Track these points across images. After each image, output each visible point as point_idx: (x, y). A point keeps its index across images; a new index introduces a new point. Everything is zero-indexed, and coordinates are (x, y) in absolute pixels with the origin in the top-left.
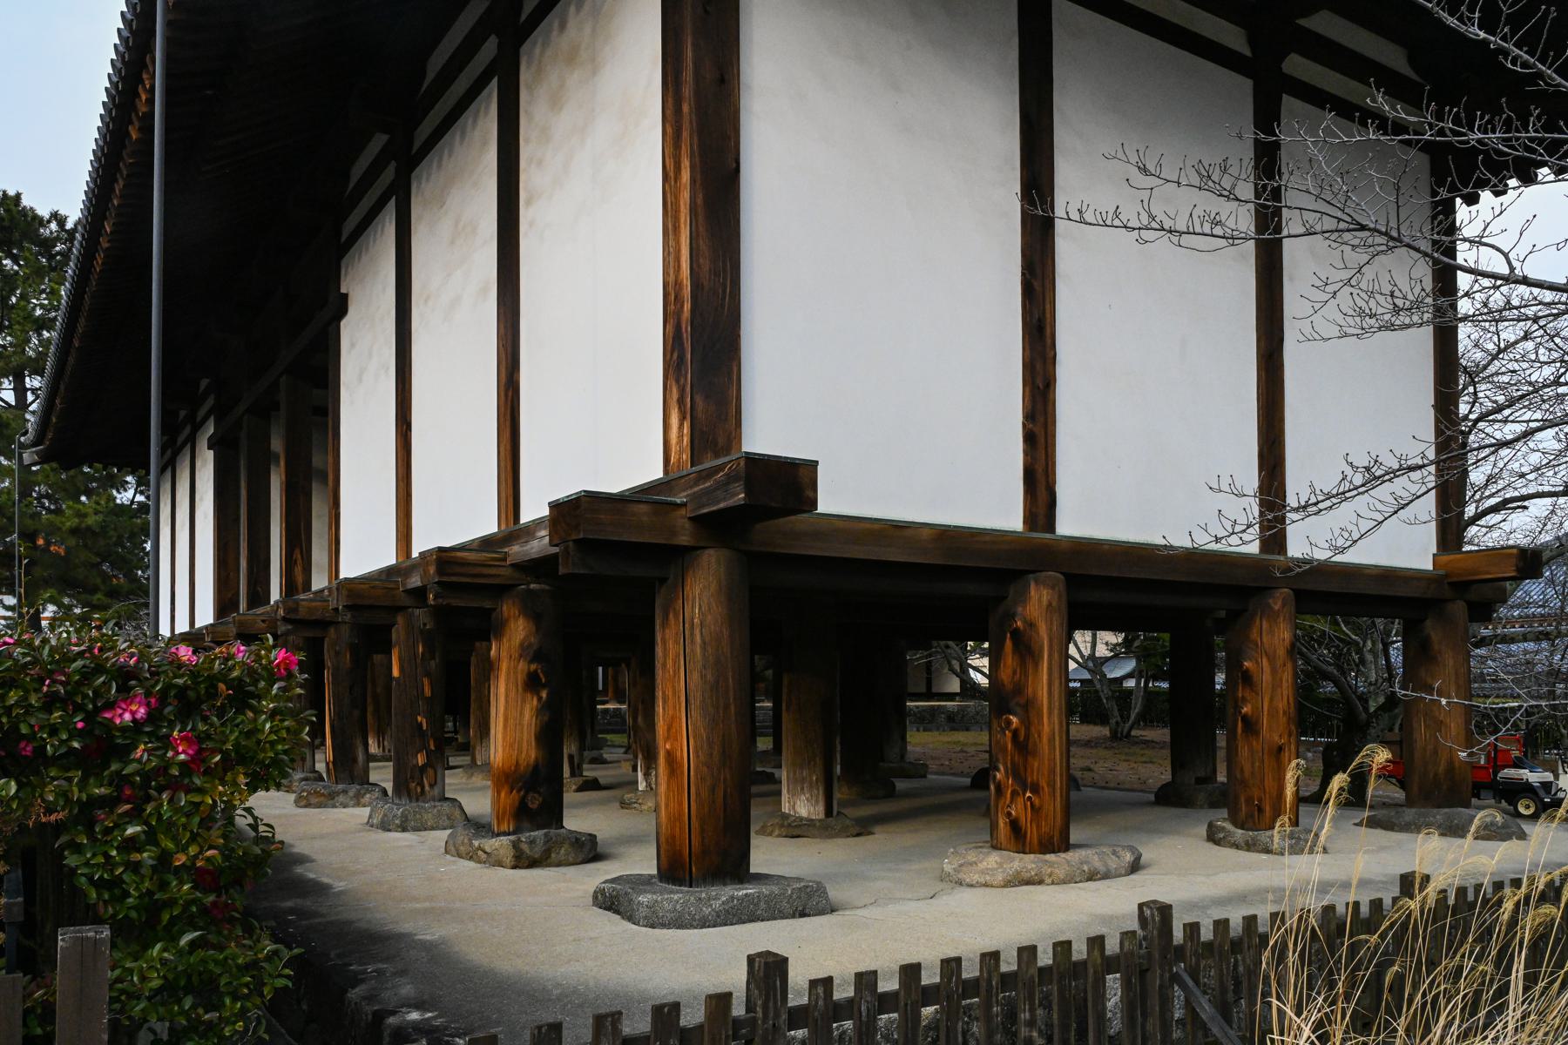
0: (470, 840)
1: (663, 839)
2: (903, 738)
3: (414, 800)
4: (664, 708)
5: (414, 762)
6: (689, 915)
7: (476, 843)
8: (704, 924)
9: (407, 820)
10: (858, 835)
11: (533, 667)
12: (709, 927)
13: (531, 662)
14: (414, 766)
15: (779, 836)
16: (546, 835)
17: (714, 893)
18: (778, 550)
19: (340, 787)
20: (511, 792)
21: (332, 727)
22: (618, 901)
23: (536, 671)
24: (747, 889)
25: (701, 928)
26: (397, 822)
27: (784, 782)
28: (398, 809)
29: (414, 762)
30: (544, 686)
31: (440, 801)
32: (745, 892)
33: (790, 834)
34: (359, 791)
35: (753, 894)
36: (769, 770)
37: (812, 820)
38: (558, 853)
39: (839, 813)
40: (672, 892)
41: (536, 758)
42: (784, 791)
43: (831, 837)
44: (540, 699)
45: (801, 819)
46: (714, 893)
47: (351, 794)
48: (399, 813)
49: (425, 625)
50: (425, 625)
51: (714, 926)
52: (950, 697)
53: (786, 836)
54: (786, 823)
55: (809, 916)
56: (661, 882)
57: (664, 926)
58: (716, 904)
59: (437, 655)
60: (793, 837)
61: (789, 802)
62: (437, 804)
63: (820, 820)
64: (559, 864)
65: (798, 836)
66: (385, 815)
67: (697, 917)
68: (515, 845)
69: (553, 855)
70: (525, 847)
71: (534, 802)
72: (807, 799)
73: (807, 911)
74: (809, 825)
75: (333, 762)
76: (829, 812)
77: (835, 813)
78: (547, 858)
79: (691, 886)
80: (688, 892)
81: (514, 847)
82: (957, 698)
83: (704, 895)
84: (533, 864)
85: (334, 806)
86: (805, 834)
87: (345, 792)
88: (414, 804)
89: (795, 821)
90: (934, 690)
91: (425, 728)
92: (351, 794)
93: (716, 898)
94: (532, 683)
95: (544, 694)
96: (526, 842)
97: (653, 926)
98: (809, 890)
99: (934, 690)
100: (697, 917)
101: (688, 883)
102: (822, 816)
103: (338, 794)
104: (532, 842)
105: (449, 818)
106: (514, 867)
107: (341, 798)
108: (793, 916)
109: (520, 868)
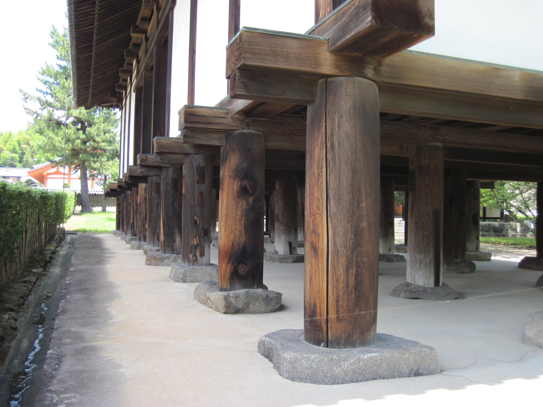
0: (205, 292)
1: (307, 305)
2: (478, 238)
3: (191, 264)
4: (310, 203)
6: (323, 372)
8: (335, 381)
9: (186, 276)
10: (456, 299)
11: (244, 183)
12: (338, 384)
13: (242, 180)
14: (192, 245)
16: (246, 293)
17: (344, 356)
19: (166, 255)
20: (229, 263)
21: (164, 223)
24: (372, 352)
25: (332, 384)
26: (181, 276)
28: (182, 269)
29: (192, 242)
30: (251, 195)
33: (410, 297)
34: (175, 258)
36: (401, 254)
38: (254, 305)
39: (443, 284)
40: (310, 352)
41: (245, 242)
43: (437, 299)
45: (419, 287)
46: (344, 356)
47: (171, 259)
49: (200, 164)
51: (343, 383)
52: (495, 219)
53: (408, 298)
55: (422, 375)
56: (305, 341)
58: (345, 365)
59: (206, 181)
60: (413, 298)
61: (411, 275)
62: (204, 267)
63: (431, 288)
64: (255, 312)
65: (416, 298)
67: (328, 375)
68: (226, 298)
69: (251, 306)
70: (232, 300)
71: (242, 269)
72: (423, 274)
73: (421, 371)
74: (424, 291)
75: (164, 242)
77: (441, 284)
78: (246, 308)
80: (323, 352)
81: (225, 299)
82: (498, 220)
84: (237, 311)
85: (163, 265)
86: (419, 297)
87: (168, 258)
88: (191, 267)
89: (414, 288)
90: (487, 216)
91: (198, 223)
92: (171, 259)
93: (346, 360)
94: (243, 192)
95: (251, 200)
96: (233, 297)
97: (293, 379)
98: (423, 354)
99: (487, 216)
100: (328, 375)
103: (165, 258)
104: (237, 297)
105: (210, 276)
106: (226, 313)
107: (166, 261)
108: (409, 376)
109: (229, 313)
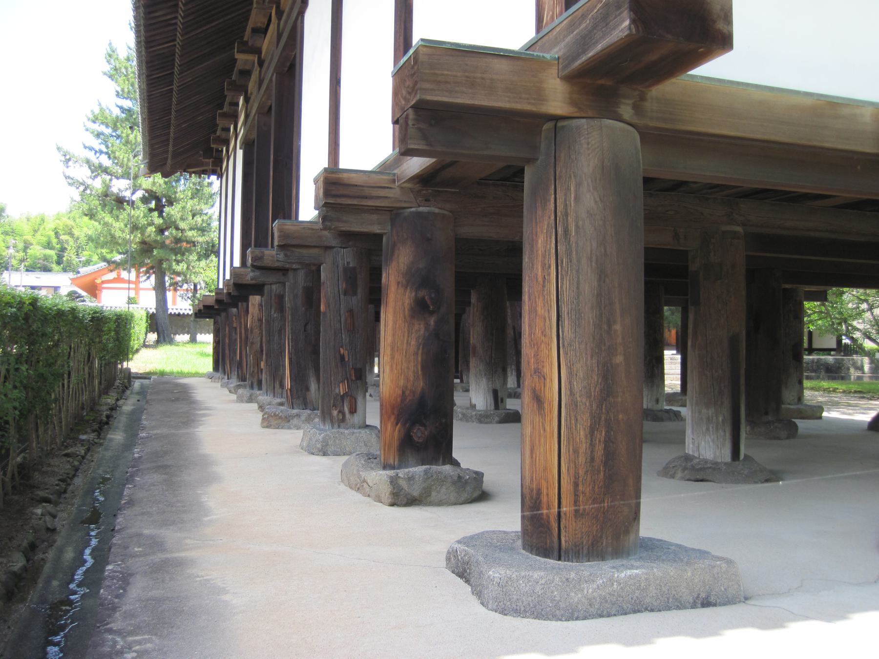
0: (358, 471)
3: (336, 426)
4: (530, 326)
5: (337, 391)
6: (552, 600)
7: (363, 474)
9: (327, 445)
10: (767, 481)
12: (577, 619)
14: (337, 395)
15: (683, 479)
16: (426, 472)
17: (586, 573)
18: (684, 128)
19: (295, 411)
20: (397, 424)
22: (470, 570)
23: (423, 298)
25: (567, 620)
26: (319, 446)
27: (689, 421)
28: (320, 434)
29: (337, 391)
30: (432, 313)
31: (360, 428)
32: (629, 572)
33: (692, 478)
34: (309, 415)
35: (637, 575)
36: (675, 408)
37: (716, 463)
38: (438, 492)
39: (746, 456)
42: (689, 432)
43: (737, 481)
44: (427, 326)
45: (706, 461)
46: (586, 573)
47: (303, 418)
48: (321, 438)
49: (348, 263)
50: (348, 263)
51: (585, 618)
52: (827, 351)
53: (689, 480)
54: (689, 464)
55: (715, 605)
57: (517, 612)
58: (589, 589)
60: (697, 481)
63: (725, 464)
64: (440, 504)
65: (702, 481)
66: (310, 439)
67: (562, 605)
68: (393, 481)
69: (434, 494)
70: (403, 483)
71: (419, 434)
73: (712, 599)
74: (714, 469)
75: (290, 390)
76: (736, 453)
77: (742, 457)
79: (559, 559)
81: (391, 482)
82: (832, 353)
83: (573, 575)
84: (411, 502)
85: (289, 428)
86: (708, 478)
87: (298, 416)
88: (335, 430)
89: (699, 463)
92: (303, 418)
94: (420, 308)
96: (404, 479)
97: (504, 612)
98: (715, 571)
100: (562, 605)
101: (556, 553)
102: (728, 458)
103: (293, 417)
104: (410, 479)
105: (366, 445)
107: (295, 421)
108: (694, 606)
109: (398, 505)
